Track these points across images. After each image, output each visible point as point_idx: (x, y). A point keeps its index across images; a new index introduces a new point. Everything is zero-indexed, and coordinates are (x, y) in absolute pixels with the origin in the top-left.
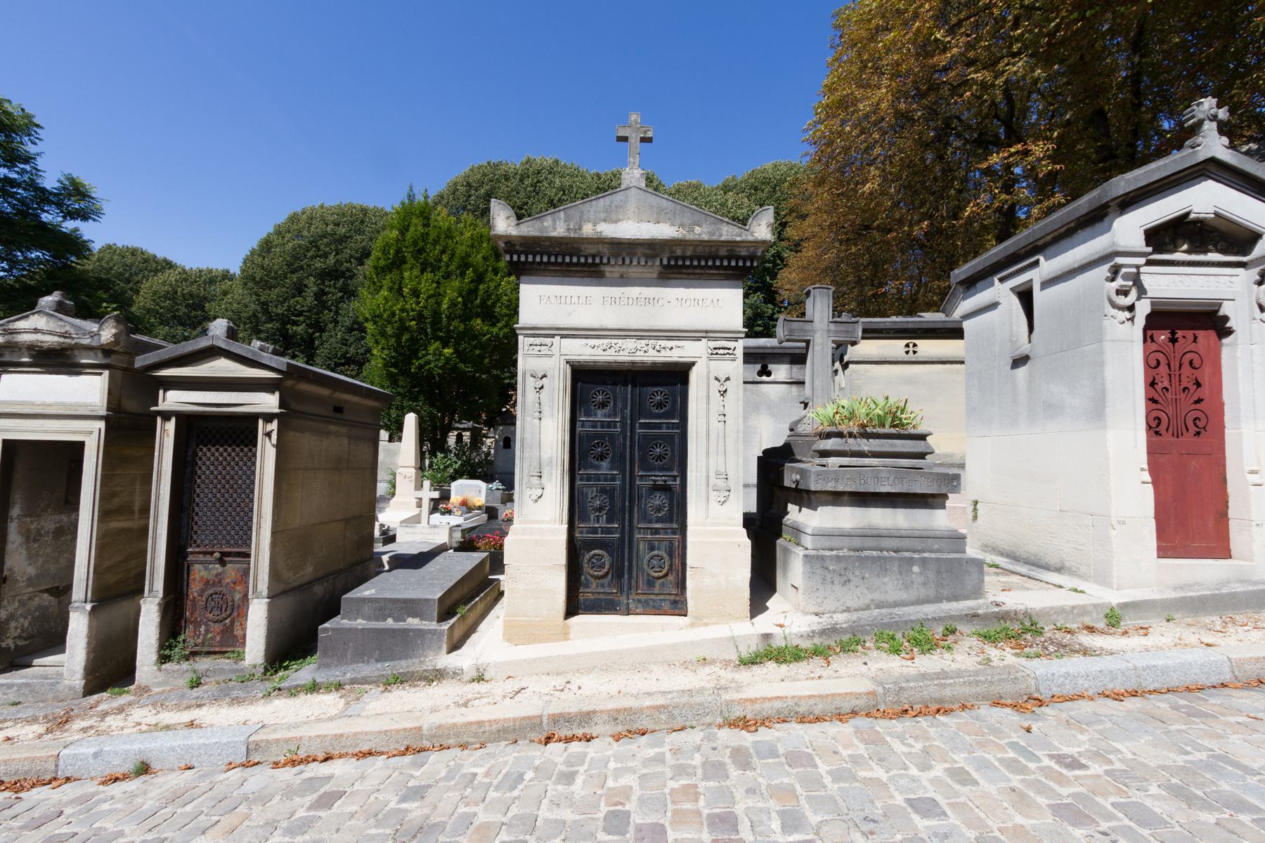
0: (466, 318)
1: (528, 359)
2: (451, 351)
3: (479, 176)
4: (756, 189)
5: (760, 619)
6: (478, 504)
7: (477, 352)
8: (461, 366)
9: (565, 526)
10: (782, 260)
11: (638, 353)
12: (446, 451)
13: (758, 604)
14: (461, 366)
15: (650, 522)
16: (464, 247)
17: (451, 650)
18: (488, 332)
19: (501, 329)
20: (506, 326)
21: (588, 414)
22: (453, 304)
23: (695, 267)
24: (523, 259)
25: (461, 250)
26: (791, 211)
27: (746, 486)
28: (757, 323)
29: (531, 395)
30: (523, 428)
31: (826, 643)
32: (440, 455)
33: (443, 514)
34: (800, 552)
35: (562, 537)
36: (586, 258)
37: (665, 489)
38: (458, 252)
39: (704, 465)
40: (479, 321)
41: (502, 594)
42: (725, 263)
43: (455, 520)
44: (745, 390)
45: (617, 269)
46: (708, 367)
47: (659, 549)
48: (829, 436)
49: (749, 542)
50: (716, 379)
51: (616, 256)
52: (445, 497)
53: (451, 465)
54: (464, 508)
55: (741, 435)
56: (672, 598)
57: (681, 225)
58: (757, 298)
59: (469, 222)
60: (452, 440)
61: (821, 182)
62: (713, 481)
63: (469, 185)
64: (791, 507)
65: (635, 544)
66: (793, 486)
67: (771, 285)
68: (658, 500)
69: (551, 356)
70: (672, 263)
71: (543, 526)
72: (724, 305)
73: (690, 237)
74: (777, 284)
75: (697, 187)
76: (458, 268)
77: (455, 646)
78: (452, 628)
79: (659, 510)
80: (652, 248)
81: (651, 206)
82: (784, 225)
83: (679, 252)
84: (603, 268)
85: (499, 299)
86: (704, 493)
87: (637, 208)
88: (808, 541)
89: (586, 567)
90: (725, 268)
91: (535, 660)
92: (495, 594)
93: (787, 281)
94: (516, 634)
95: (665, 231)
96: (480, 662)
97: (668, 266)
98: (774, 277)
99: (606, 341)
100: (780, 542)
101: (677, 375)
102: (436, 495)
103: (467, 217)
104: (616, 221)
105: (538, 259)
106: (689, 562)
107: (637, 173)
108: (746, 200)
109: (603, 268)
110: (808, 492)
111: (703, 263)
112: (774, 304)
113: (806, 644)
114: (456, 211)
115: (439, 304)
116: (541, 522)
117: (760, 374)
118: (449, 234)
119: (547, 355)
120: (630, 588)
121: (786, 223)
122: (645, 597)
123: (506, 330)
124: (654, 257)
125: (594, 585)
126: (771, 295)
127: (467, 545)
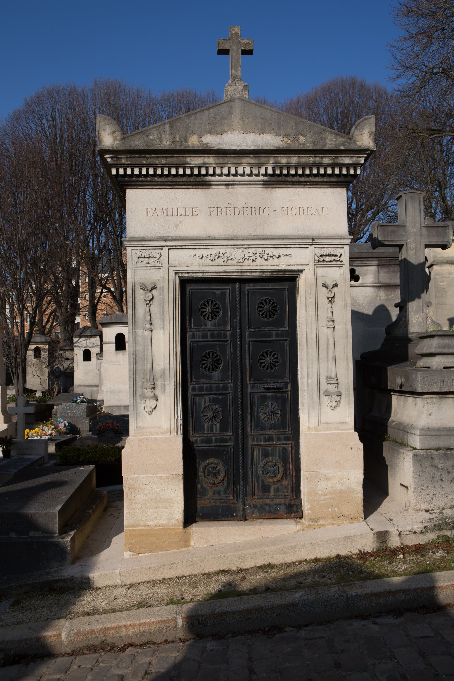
1: (137, 273)
11: (246, 262)
36: (192, 169)
39: (315, 370)
42: (329, 171)
46: (316, 274)
50: (325, 286)
57: (286, 135)
62: (324, 386)
65: (249, 452)
69: (160, 268)
70: (278, 172)
88: (416, 441)
99: (214, 251)
120: (245, 494)
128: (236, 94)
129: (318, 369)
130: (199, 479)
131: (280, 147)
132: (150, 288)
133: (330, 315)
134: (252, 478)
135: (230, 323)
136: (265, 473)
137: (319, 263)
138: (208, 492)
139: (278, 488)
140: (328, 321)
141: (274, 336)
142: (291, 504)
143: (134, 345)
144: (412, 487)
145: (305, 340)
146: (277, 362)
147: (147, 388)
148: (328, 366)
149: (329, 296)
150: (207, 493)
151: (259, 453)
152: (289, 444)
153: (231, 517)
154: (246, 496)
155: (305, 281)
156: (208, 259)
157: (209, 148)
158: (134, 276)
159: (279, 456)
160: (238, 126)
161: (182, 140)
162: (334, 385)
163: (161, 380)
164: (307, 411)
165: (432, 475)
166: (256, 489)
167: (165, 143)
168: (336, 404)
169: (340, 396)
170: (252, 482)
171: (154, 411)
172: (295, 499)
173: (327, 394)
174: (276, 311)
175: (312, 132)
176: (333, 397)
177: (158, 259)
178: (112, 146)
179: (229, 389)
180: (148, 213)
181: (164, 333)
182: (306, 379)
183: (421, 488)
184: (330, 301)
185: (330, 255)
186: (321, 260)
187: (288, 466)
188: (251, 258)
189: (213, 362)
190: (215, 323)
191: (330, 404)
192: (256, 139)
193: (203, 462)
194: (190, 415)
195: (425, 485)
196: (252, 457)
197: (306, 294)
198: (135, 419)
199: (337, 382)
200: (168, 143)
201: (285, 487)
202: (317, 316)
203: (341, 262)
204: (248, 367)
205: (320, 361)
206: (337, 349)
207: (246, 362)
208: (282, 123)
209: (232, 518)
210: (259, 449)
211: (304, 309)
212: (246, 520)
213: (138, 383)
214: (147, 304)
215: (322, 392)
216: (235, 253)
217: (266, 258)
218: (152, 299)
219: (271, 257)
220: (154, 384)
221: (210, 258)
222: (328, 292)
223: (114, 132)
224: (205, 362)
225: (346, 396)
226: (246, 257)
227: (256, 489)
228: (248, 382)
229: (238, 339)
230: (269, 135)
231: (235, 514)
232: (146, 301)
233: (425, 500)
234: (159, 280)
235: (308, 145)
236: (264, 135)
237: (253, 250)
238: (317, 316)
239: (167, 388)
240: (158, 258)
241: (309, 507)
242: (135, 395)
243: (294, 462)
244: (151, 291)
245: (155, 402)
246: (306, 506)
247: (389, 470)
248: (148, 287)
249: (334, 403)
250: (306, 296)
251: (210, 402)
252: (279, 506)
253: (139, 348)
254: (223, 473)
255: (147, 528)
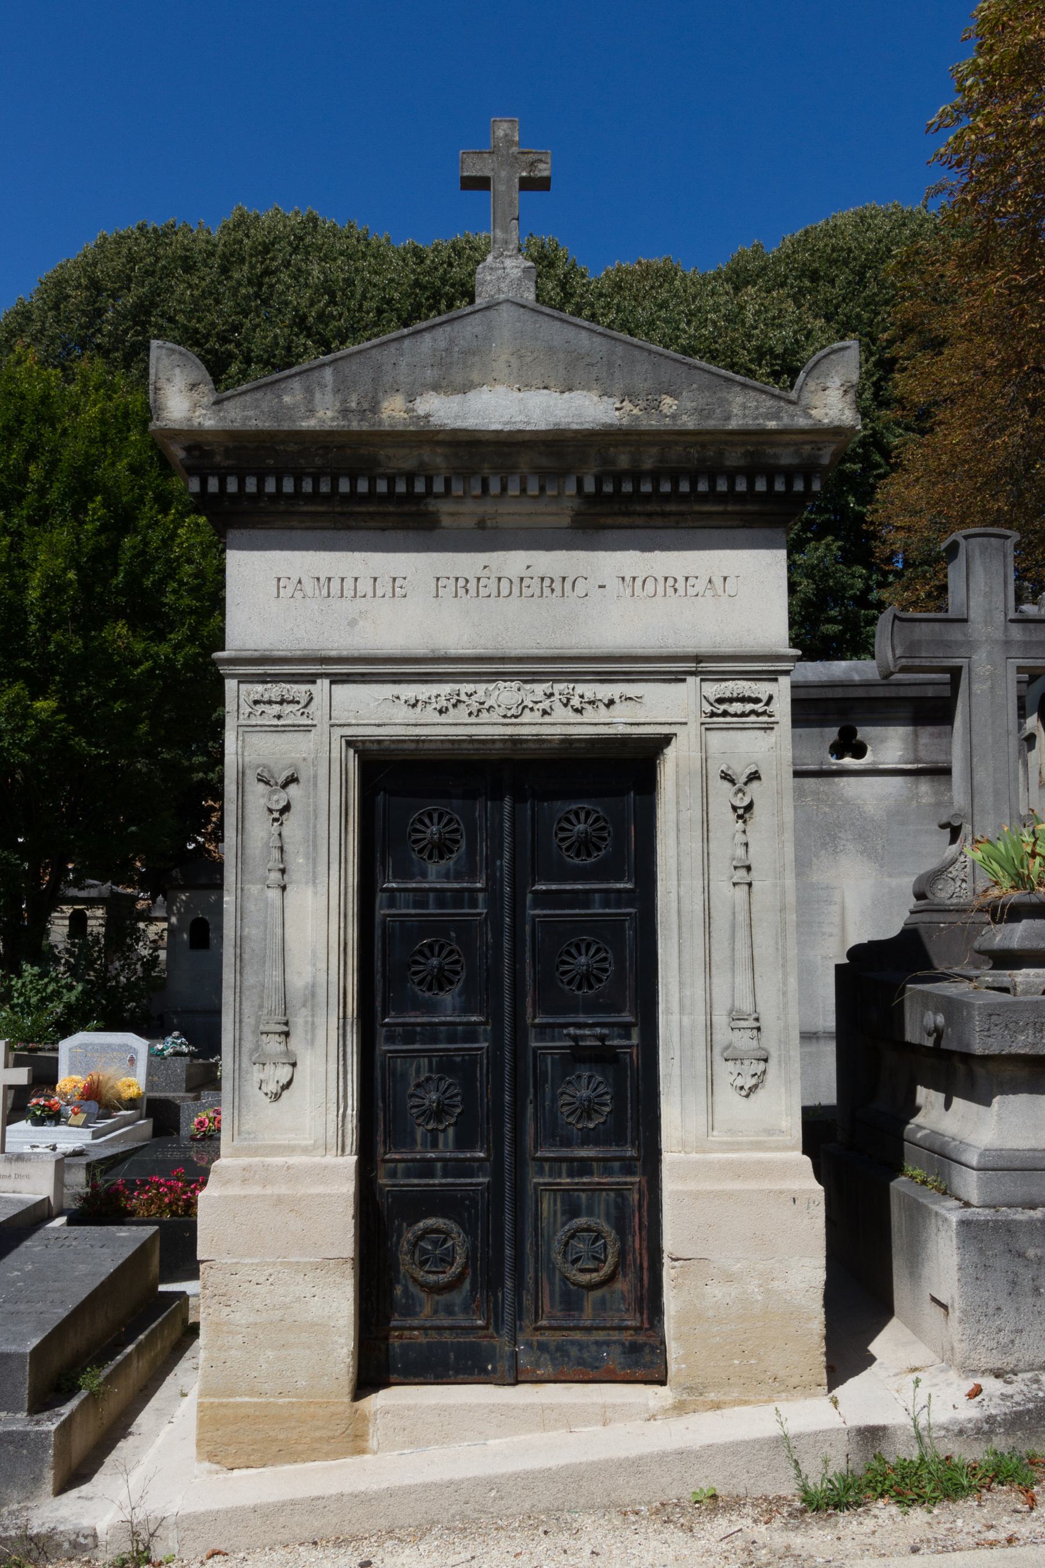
0: (90, 619)
1: (252, 739)
2: (52, 704)
3: (118, 263)
4: (815, 277)
5: (851, 1389)
6: (131, 1093)
7: (118, 707)
8: (80, 743)
9: (351, 1160)
10: (886, 452)
11: (527, 717)
12: (44, 957)
13: (846, 1354)
14: (80, 743)
15: (567, 1142)
16: (81, 446)
17: (61, 1489)
18: (146, 655)
19: (178, 647)
20: (191, 639)
21: (403, 874)
22: (54, 588)
23: (666, 498)
24: (232, 487)
25: (73, 451)
26: (907, 329)
27: (808, 1037)
28: (822, 621)
29: (260, 830)
30: (241, 913)
31: (1025, 1449)
32: (29, 970)
33: (39, 1122)
34: (952, 1214)
35: (344, 1187)
36: (391, 481)
37: (603, 1057)
38: (66, 454)
39: (700, 993)
40: (121, 628)
41: (192, 1331)
42: (741, 486)
43: (70, 1138)
44: (799, 794)
45: (469, 507)
46: (704, 747)
47: (590, 1213)
48: (1015, 913)
49: (818, 1190)
50: (726, 777)
51: (466, 474)
52: (45, 1077)
53: (57, 994)
54: (93, 1106)
55: (792, 917)
56: (627, 1337)
57: (629, 395)
58: (822, 551)
59: (94, 378)
60: (59, 930)
61: (983, 258)
62: (723, 1035)
63: (95, 286)
64: (923, 1095)
65: (530, 1203)
66: (929, 1042)
67: (860, 517)
68: (586, 1086)
69: (307, 729)
70: (608, 488)
71: (294, 1160)
72: (739, 593)
73: (652, 423)
74: (874, 514)
75: (666, 276)
76: (65, 496)
77: (76, 1474)
78: (66, 1427)
79: (588, 1110)
80: (551, 454)
81: (551, 350)
82: (887, 366)
83: (623, 462)
84: (433, 505)
85: (171, 572)
86: (701, 1065)
87: (517, 353)
88: (970, 1184)
89: (406, 1262)
90: (741, 498)
91: (279, 1508)
92: (174, 1334)
93: (900, 505)
94: (228, 1441)
95: (587, 409)
96: (140, 1515)
97: (598, 497)
98: (866, 496)
99: (446, 689)
100: (899, 1185)
101: (629, 767)
102: (21, 1076)
103: (90, 367)
104: (465, 388)
105: (270, 486)
106: (669, 1243)
107: (515, 266)
108: (790, 305)
109: (433, 505)
110: (967, 1057)
111: (684, 487)
112: (868, 566)
113: (974, 1453)
114: (61, 360)
115: (20, 588)
116: (291, 1150)
117: (839, 750)
118: (45, 411)
119: (297, 728)
120: (519, 1314)
121: (894, 360)
122: (557, 1337)
123: (191, 650)
124: (560, 474)
125: (426, 1311)
126: (860, 544)
127: (99, 1207)
128: (505, 289)
129: (709, 990)
130: (399, 1272)
131: (612, 425)
132: (281, 780)
133: (740, 852)
134: (536, 1271)
135: (487, 868)
136: (570, 1259)
137: (715, 719)
138: (420, 1305)
139: (603, 1301)
140: (736, 868)
141: (597, 905)
143: (239, 922)
144: (956, 1306)
145: (676, 915)
146: (606, 970)
147: (267, 1033)
148: (733, 982)
149: (738, 804)
150: (418, 1309)
151: (555, 1204)
152: (632, 1184)
153: (479, 1374)
154: (521, 1319)
155: (677, 766)
156: (430, 708)
157: (433, 428)
158: (243, 747)
160: (506, 371)
161: (366, 406)
162: (749, 1033)
163: (304, 1012)
164: (678, 1099)
165: (1011, 1276)
166: (547, 1300)
167: (320, 414)
168: (754, 1081)
169: (766, 1060)
170: (536, 1283)
171: (285, 1093)
172: (647, 1330)
173: (733, 1058)
174: (604, 839)
175: (695, 386)
176: (747, 1062)
177: (305, 707)
178: (190, 420)
179: (481, 1038)
180: (281, 590)
181: (315, 893)
182: (676, 1017)
183: (980, 1310)
184: (740, 817)
185: (743, 700)
186: (719, 714)
187: (630, 1243)
188: (541, 706)
189: (441, 969)
190: (449, 870)
191: (739, 1082)
192: (552, 403)
193: (410, 1225)
194: (381, 1104)
195: (992, 1304)
196: (537, 1214)
197: (678, 797)
198: (236, 1112)
199: (756, 1024)
200: (329, 414)
201: (623, 1298)
202: (707, 855)
203: (770, 716)
204: (529, 981)
205: (713, 969)
206: (758, 939)
207: (525, 969)
208: (619, 362)
209: (482, 1377)
211: (673, 835)
212: (516, 1382)
213: (245, 1020)
214: (275, 820)
215: (717, 1050)
216: (497, 692)
217: (578, 706)
218: (286, 809)
219: (589, 703)
220: (286, 1024)
221: (434, 705)
222: (736, 794)
223: (193, 386)
224: (421, 968)
225: (780, 1061)
226: (525, 703)
227: (547, 1300)
228: (529, 1021)
229: (507, 911)
230: (585, 393)
231: (490, 1367)
232: (271, 811)
233: (993, 1344)
234: (304, 759)
235: (685, 418)
236: (573, 394)
237: (545, 687)
238: (707, 855)
239: (321, 1034)
240: (303, 703)
241: (682, 1352)
242: (237, 1049)
243: (644, 1233)
244: (285, 786)
245: (288, 1069)
246: (674, 1350)
247: (895, 1278)
248: (276, 775)
249: (749, 1078)
250: (678, 803)
251: (430, 1070)
252: (604, 1348)
253: (252, 932)
254: (459, 1260)
255: (255, 1400)
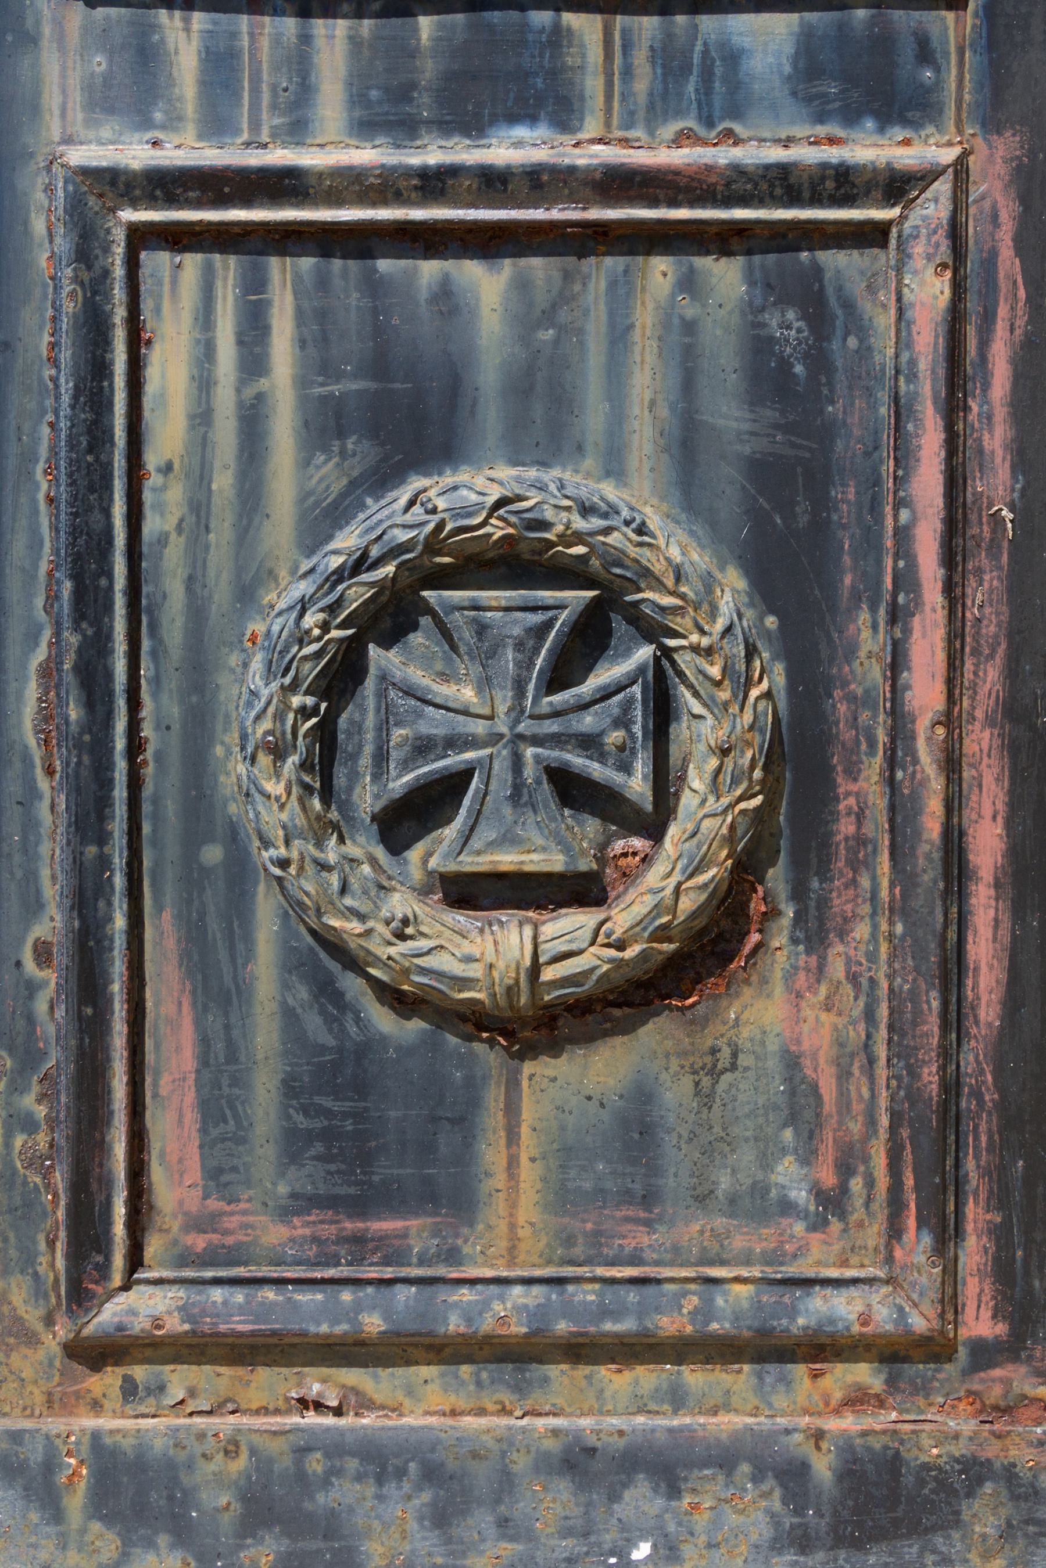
136: (367, 799)
142: (892, 1463)
159: (687, 446)
172: (984, 1356)
201: (800, 1106)
210: (255, 285)
243: (986, 592)
